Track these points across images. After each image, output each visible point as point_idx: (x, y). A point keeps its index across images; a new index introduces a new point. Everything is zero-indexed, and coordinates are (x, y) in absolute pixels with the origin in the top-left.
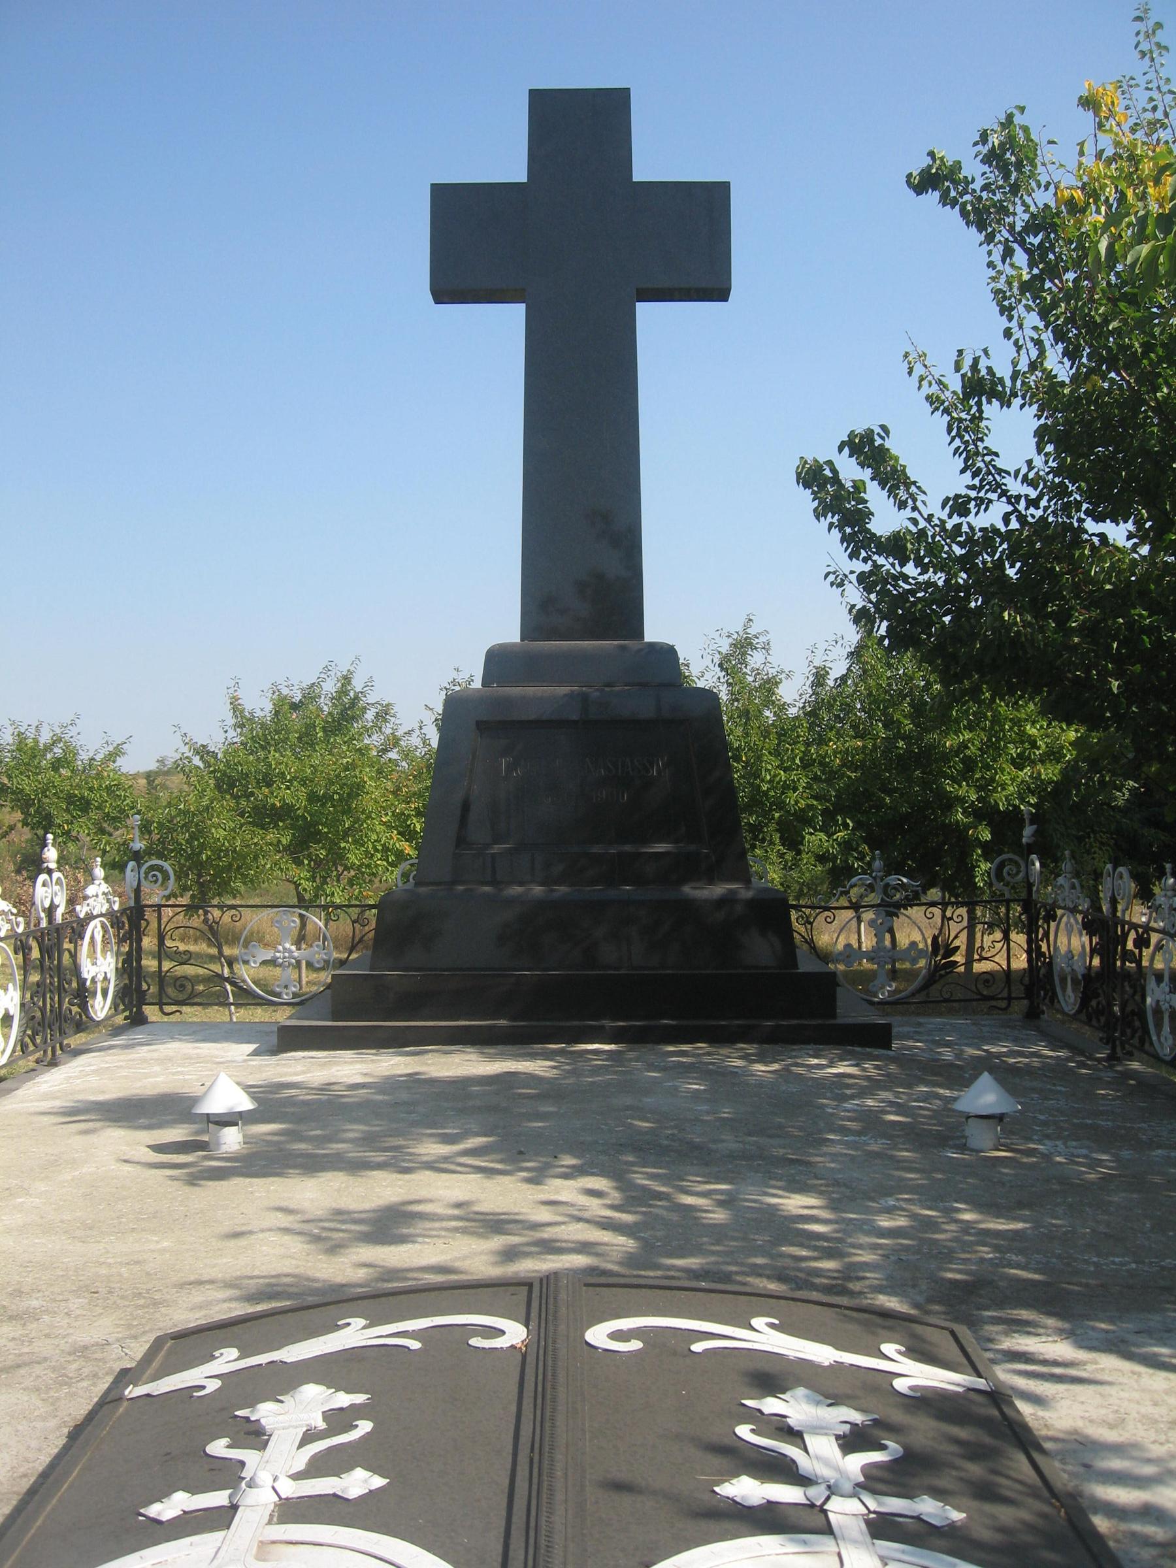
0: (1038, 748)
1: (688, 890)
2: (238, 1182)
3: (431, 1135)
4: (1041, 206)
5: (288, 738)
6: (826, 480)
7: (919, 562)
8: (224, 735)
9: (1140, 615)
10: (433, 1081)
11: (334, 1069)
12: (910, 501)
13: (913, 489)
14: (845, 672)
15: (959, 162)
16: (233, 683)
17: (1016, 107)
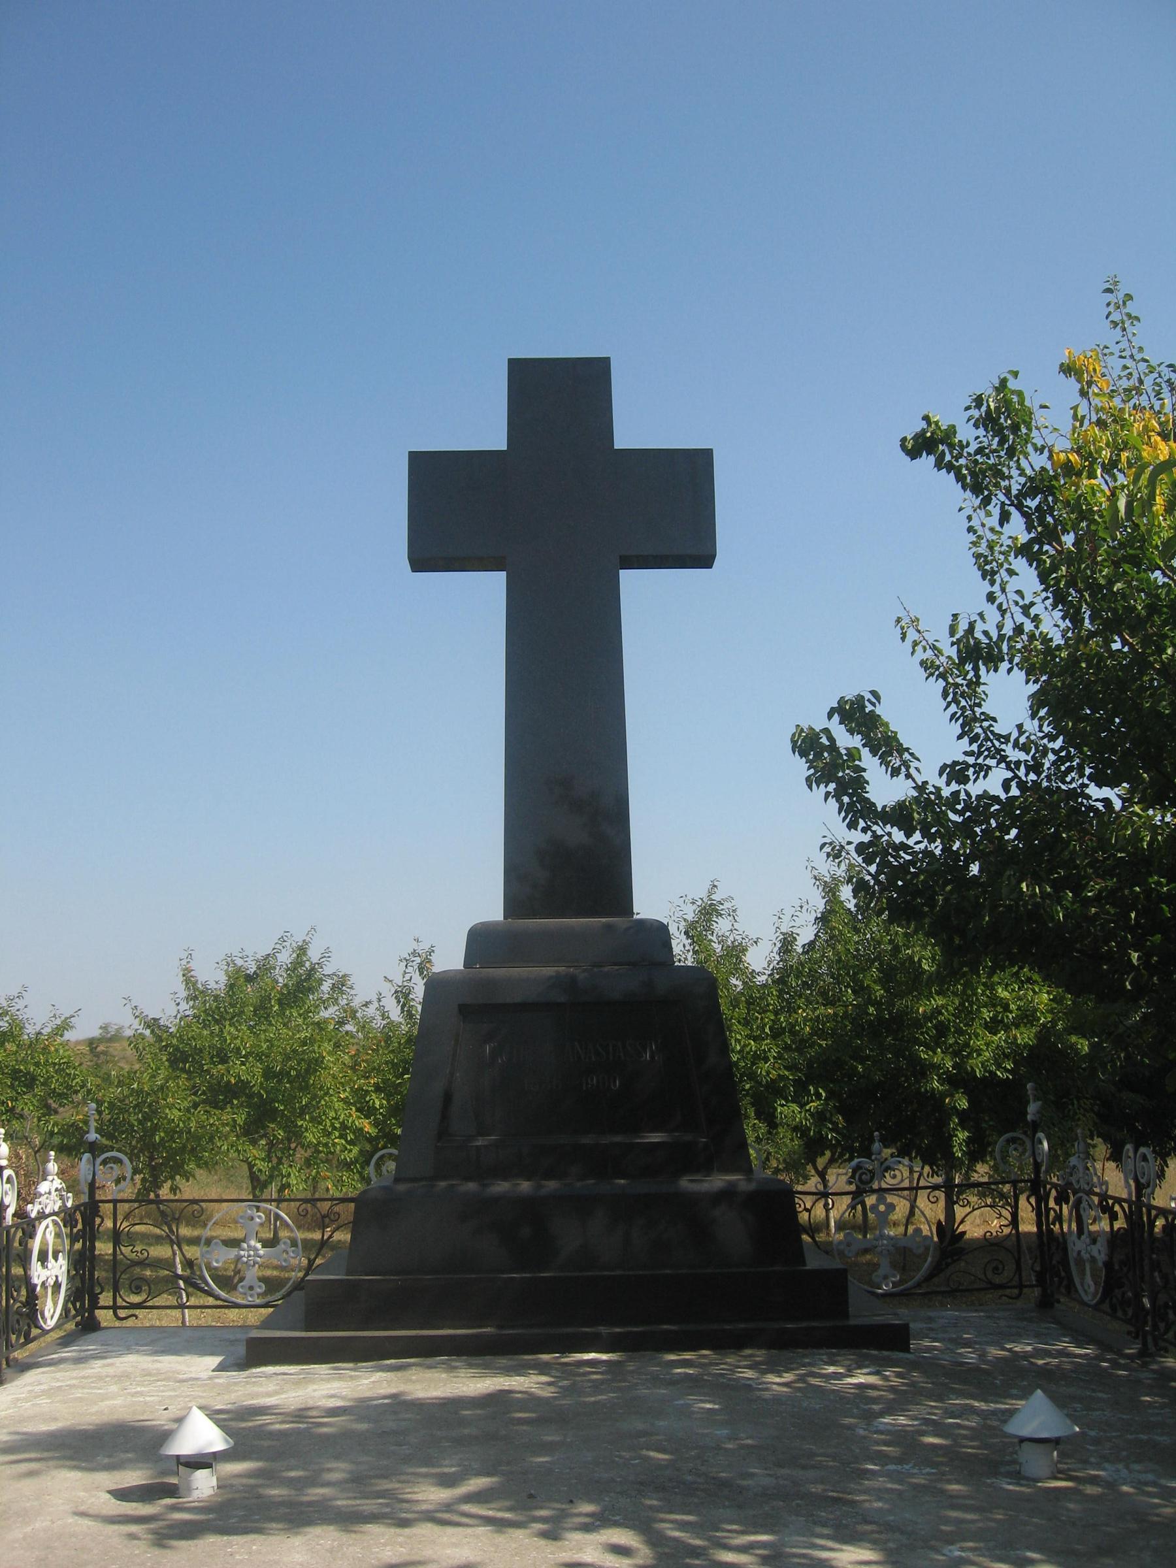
0: (1011, 1012)
1: (686, 1184)
2: (211, 1542)
3: (426, 1476)
4: (1037, 469)
5: (243, 1012)
6: (824, 748)
7: (926, 834)
8: (175, 1008)
9: (1158, 883)
10: (418, 1406)
11: (311, 1387)
12: (903, 769)
13: (906, 756)
14: (812, 938)
15: (954, 426)
16: (186, 954)
17: (1010, 372)
